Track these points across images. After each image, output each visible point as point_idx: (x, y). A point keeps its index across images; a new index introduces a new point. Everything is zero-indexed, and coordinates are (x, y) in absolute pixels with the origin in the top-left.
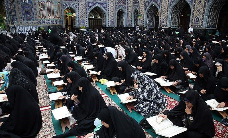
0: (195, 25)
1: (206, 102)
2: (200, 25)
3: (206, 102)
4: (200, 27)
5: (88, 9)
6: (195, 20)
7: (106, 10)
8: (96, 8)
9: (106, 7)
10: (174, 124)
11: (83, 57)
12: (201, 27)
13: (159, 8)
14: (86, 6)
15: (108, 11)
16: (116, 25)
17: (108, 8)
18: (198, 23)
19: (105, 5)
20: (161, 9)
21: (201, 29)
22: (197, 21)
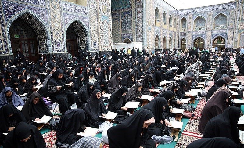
0: (57, 49)
1: (239, 123)
2: (63, 49)
3: (239, 123)
4: (63, 51)
5: (212, 38)
6: (56, 44)
7: (226, 38)
8: (24, 15)
9: (226, 36)
10: (108, 131)
11: (186, 92)
12: (64, 51)
13: (204, 39)
14: (62, 18)
15: (90, 28)
16: (66, 49)
17: (89, 25)
18: (60, 47)
19: (225, 35)
20: (91, 31)
21: (65, 53)
22: (58, 45)
